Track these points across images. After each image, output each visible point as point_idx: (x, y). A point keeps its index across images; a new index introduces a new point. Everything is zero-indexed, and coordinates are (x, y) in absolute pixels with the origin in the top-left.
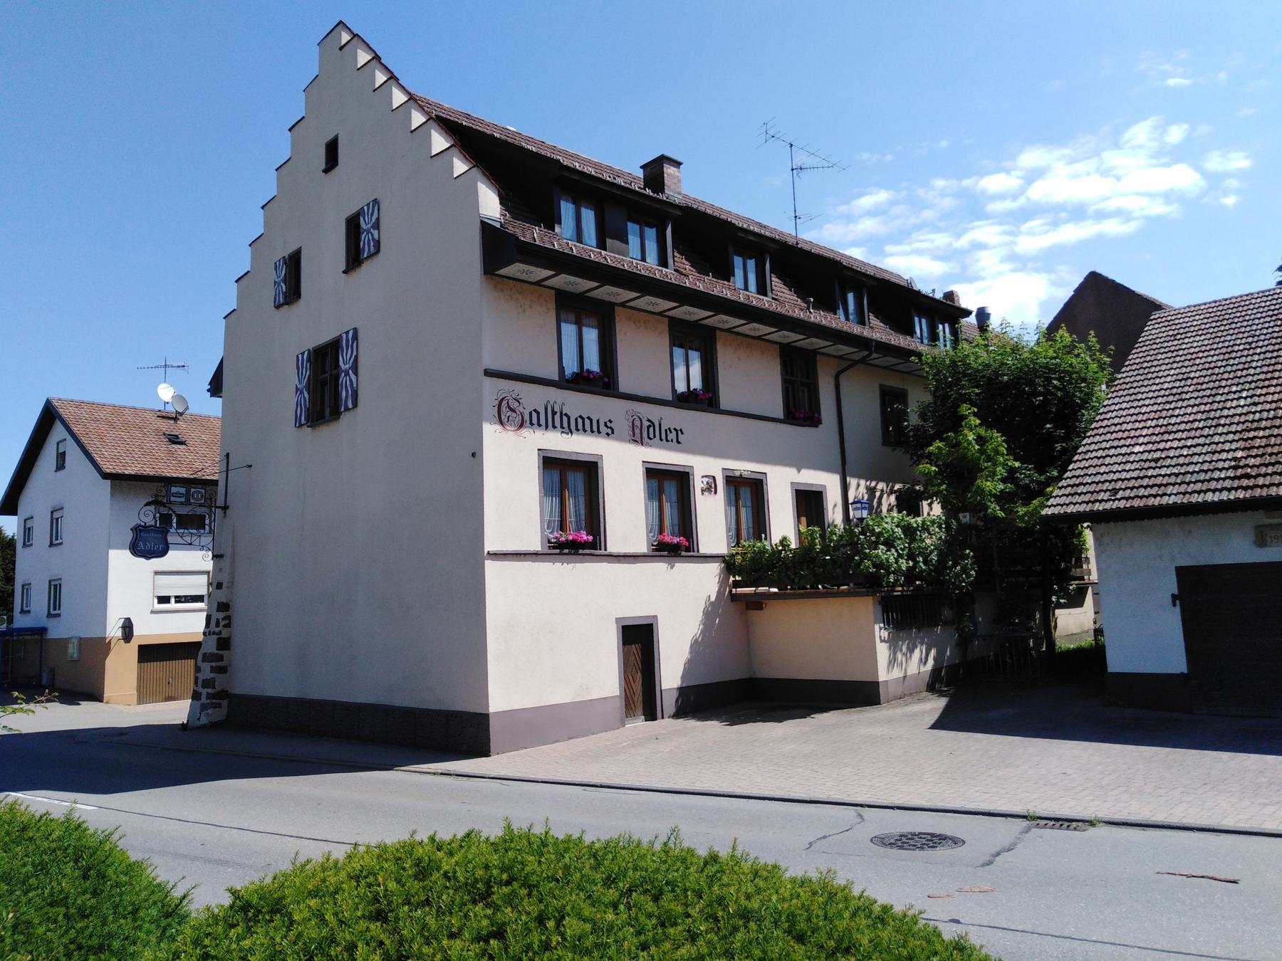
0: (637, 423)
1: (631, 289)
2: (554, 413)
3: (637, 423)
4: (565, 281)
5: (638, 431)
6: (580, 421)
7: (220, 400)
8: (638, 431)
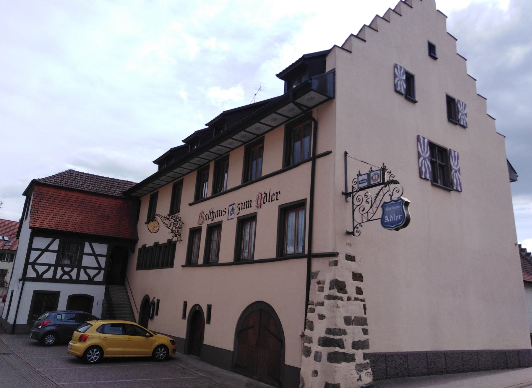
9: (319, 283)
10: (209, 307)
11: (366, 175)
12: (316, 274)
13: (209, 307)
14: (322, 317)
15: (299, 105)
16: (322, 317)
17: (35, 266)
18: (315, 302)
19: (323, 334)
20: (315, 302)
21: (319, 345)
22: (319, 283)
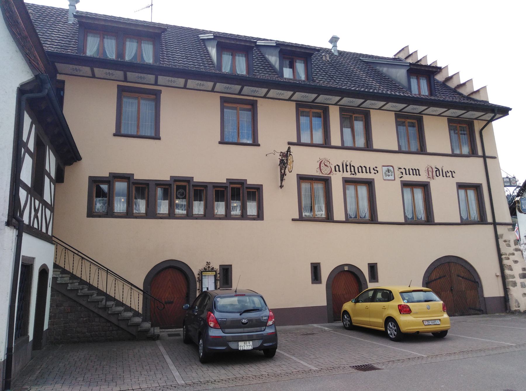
0: (430, 169)
1: (359, 98)
2: (347, 166)
3: (430, 169)
4: (298, 96)
5: (430, 174)
6: (360, 168)
7: (504, 175)
8: (430, 174)
9: (505, 241)
10: (373, 268)
11: (460, 191)
12: (502, 236)
13: (373, 268)
14: (516, 262)
15: (281, 67)
16: (516, 262)
17: (56, 64)
18: (508, 253)
19: (521, 272)
20: (508, 253)
21: (521, 278)
22: (505, 241)
